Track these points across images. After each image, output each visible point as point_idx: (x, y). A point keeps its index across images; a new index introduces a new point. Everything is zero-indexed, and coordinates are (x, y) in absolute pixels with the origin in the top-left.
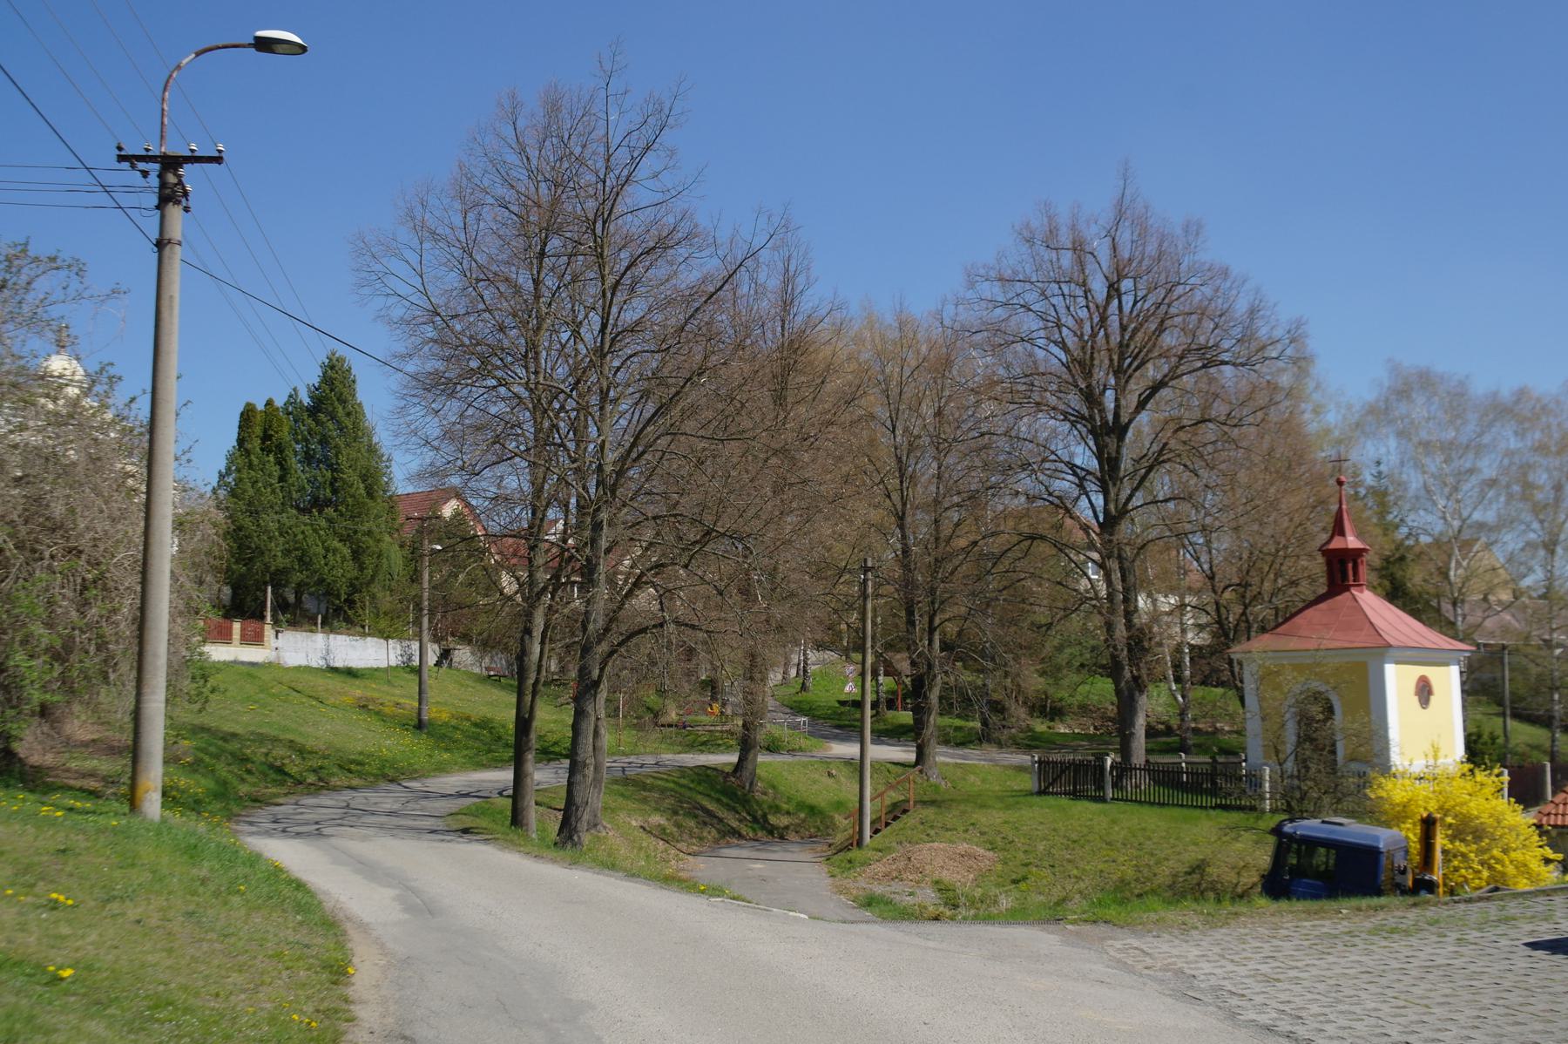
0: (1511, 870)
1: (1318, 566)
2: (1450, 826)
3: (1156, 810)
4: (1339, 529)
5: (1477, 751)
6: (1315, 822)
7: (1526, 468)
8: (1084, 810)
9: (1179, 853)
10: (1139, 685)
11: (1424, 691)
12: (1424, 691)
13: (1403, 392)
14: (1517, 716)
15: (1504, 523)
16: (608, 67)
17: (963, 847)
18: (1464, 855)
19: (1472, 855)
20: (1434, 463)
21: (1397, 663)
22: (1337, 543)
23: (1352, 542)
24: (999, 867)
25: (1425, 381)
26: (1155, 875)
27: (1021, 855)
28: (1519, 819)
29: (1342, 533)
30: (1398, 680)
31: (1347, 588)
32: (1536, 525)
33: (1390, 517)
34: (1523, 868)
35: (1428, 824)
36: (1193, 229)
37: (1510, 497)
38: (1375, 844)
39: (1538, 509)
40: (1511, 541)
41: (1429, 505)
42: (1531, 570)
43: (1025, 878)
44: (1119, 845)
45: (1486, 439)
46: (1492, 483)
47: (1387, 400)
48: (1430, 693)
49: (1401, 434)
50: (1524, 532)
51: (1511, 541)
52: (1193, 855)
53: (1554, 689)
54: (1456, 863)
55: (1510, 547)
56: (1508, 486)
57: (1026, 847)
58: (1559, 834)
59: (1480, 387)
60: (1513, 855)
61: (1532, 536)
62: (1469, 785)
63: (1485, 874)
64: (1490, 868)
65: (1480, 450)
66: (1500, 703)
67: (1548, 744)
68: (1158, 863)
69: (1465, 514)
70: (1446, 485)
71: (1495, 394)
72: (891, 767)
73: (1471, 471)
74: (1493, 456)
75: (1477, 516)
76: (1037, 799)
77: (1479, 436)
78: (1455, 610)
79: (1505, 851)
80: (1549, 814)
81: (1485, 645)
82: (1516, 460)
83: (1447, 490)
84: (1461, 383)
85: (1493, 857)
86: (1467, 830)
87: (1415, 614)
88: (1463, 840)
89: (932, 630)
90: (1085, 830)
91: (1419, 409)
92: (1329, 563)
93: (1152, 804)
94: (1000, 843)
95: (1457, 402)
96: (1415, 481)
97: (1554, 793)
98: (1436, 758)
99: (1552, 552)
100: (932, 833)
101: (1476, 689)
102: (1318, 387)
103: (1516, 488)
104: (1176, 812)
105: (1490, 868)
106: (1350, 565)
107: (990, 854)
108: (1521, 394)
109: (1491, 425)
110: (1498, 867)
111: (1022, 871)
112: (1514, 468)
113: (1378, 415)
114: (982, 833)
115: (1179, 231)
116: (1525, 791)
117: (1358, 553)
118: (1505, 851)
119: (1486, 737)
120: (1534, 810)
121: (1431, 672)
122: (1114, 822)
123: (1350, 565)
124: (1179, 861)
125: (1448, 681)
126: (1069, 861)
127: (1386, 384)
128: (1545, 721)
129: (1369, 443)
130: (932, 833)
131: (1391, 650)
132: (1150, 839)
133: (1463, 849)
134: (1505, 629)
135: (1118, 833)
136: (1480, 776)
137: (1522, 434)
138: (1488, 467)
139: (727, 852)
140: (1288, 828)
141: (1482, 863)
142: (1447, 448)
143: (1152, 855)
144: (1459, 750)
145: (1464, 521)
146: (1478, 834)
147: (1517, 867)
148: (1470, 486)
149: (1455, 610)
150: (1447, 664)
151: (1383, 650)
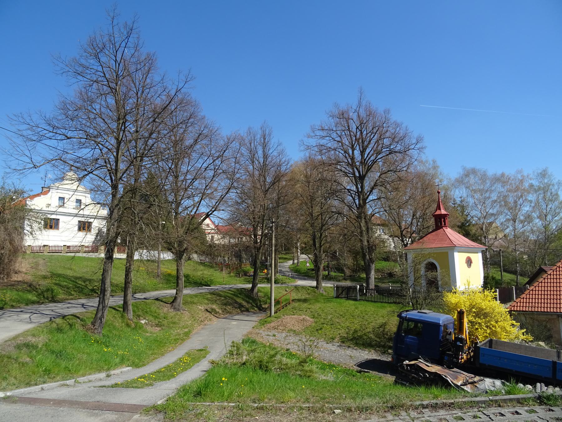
0: (499, 330)
1: (432, 221)
2: (474, 312)
3: (373, 303)
4: (439, 208)
5: (488, 283)
6: (415, 312)
7: (505, 197)
8: (350, 304)
9: (376, 320)
10: (371, 261)
11: (469, 262)
12: (469, 262)
13: (467, 175)
14: (505, 271)
15: (499, 213)
16: (112, 14)
17: (302, 317)
18: (479, 323)
19: (483, 324)
20: (478, 196)
21: (459, 252)
22: (438, 212)
23: (443, 212)
24: (314, 324)
25: (474, 171)
26: (367, 328)
27: (322, 320)
28: (501, 308)
29: (440, 209)
30: (459, 258)
31: (442, 228)
32: (509, 213)
33: (465, 213)
34: (504, 329)
35: (461, 314)
36: (387, 111)
37: (500, 206)
38: (438, 322)
39: (509, 209)
40: (502, 219)
41: (476, 208)
42: (508, 227)
43: (321, 329)
44: (356, 317)
45: (493, 188)
46: (495, 201)
47: (462, 178)
48: (471, 262)
49: (467, 188)
50: (506, 216)
51: (502, 219)
52: (381, 321)
53: (516, 263)
54: (477, 327)
55: (502, 220)
56: (500, 202)
57: (325, 317)
58: (518, 314)
59: (491, 172)
60: (499, 323)
61: (508, 217)
62: (482, 295)
63: (488, 331)
64: (490, 328)
65: (491, 191)
66: (500, 267)
67: (516, 279)
68: (368, 324)
69: (487, 211)
70: (481, 202)
71: (495, 175)
72: (309, 288)
73: (489, 198)
74: (495, 193)
75: (491, 211)
76: (334, 300)
77: (491, 187)
78: (485, 240)
79: (497, 322)
80: (514, 306)
81: (496, 251)
82: (502, 194)
83: (481, 204)
84: (484, 172)
85: (491, 324)
86: (481, 313)
87: (473, 240)
88: (479, 317)
89: (321, 246)
90: (345, 311)
91: (472, 179)
92: (435, 220)
93: (372, 301)
94: (316, 316)
95: (484, 178)
96: (471, 201)
97: (516, 299)
98: (469, 285)
99: (515, 222)
100: (295, 312)
101: (486, 263)
102: (441, 174)
103: (503, 203)
104: (379, 304)
105: (490, 328)
106: (443, 220)
107: (311, 320)
108: (503, 175)
109: (495, 183)
110: (494, 329)
111: (321, 326)
112: (502, 197)
113: (460, 182)
114: (311, 312)
115: (383, 113)
116: (505, 298)
117: (445, 216)
118: (497, 322)
119: (490, 278)
120: (508, 305)
121: (471, 255)
122: (356, 308)
123: (443, 220)
124: (376, 323)
125: (477, 258)
126: (338, 323)
127: (462, 173)
128: (514, 273)
129: (457, 191)
130: (295, 312)
131: (456, 248)
132: (367, 314)
133: (480, 321)
134: (501, 246)
135: (357, 312)
136: (487, 293)
137: (503, 186)
138: (494, 196)
139: (237, 317)
140: (404, 315)
141: (487, 327)
142: (481, 191)
143: (367, 321)
144: (481, 281)
145: (487, 213)
146: (486, 315)
147: (501, 328)
148: (488, 202)
149: (485, 240)
150: (477, 253)
151: (453, 247)
